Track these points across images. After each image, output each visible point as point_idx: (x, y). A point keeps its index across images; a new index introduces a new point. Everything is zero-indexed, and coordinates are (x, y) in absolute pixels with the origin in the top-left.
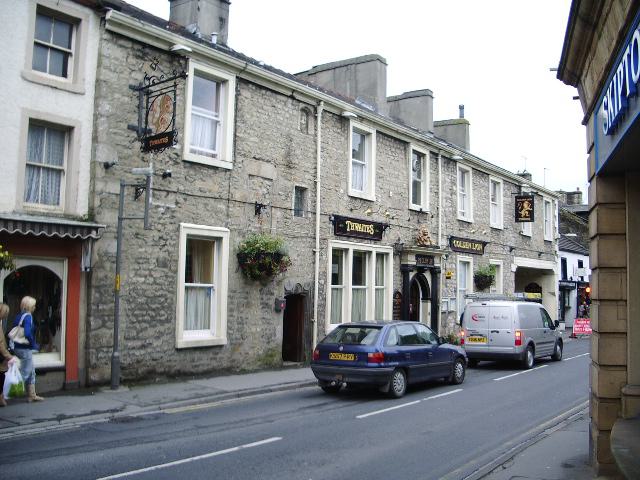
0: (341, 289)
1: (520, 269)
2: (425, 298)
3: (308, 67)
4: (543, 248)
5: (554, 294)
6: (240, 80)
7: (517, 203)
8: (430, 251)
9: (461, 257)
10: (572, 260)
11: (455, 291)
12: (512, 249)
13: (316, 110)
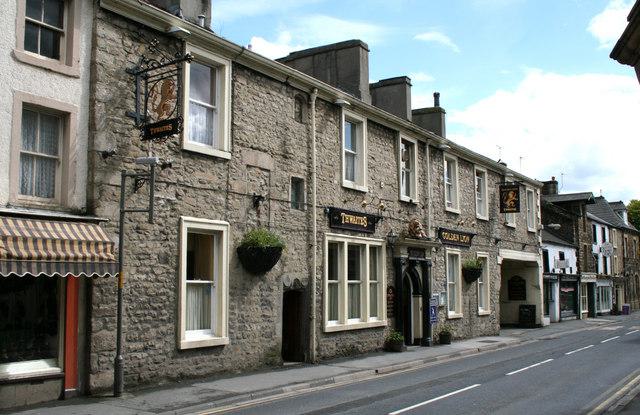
0: (336, 284)
1: (506, 262)
2: (416, 294)
3: (285, 54)
4: (526, 240)
5: (538, 288)
6: (369, 121)
7: (501, 193)
8: (421, 243)
9: (449, 250)
10: (554, 252)
11: (445, 285)
12: (497, 241)
13: (309, 99)
